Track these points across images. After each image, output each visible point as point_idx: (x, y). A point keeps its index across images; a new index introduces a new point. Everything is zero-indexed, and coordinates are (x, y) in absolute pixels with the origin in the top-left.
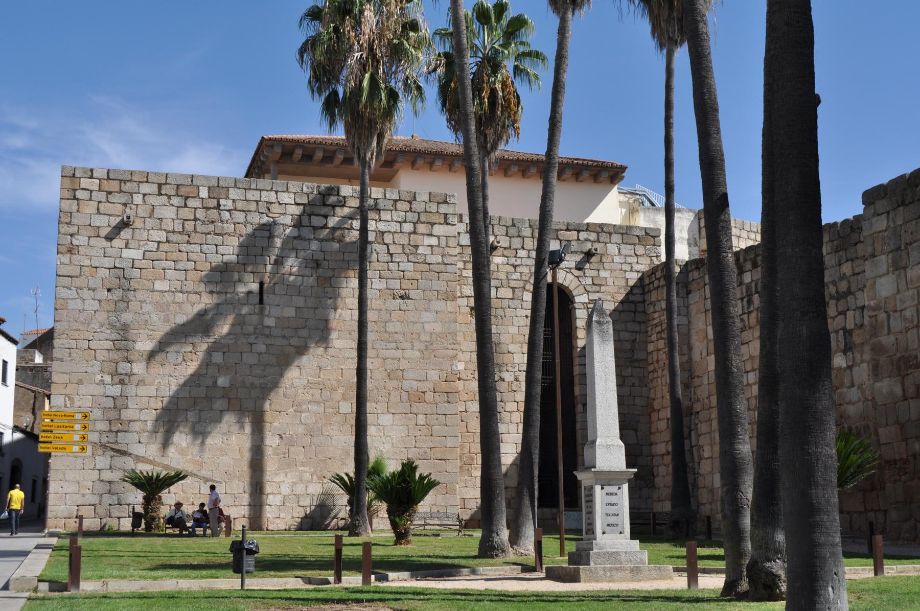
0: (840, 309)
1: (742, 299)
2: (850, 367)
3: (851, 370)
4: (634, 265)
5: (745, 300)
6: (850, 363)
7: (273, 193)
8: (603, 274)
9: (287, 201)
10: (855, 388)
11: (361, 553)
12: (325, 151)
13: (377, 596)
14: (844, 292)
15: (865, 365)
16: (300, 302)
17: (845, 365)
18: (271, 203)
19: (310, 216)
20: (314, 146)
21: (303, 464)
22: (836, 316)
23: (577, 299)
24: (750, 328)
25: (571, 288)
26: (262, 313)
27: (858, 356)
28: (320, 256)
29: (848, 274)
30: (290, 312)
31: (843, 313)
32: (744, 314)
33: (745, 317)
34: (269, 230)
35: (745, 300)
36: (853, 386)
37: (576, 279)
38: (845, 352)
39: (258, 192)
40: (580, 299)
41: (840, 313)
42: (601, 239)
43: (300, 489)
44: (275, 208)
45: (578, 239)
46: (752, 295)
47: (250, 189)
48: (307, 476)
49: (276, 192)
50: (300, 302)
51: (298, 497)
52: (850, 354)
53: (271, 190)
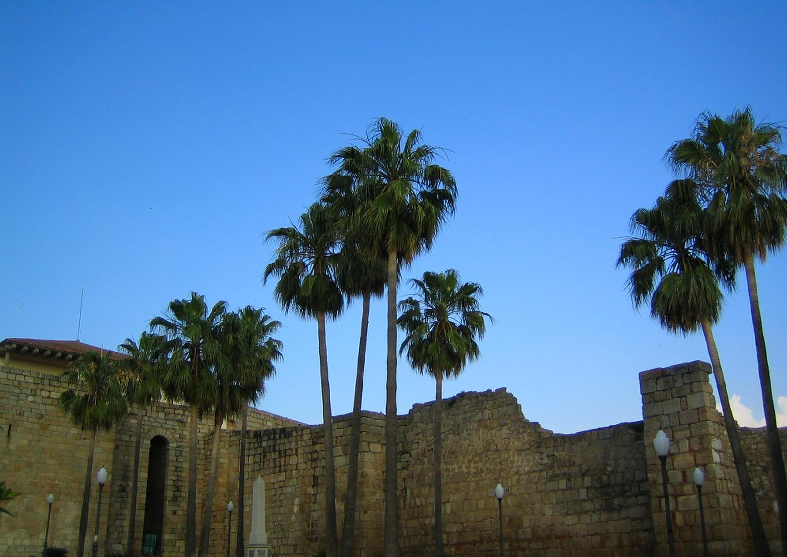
0: (313, 466)
1: (260, 454)
2: (315, 494)
3: (316, 496)
4: (201, 429)
5: (262, 455)
6: (316, 492)
7: (23, 377)
8: (185, 433)
9: (152, 421)
10: (317, 504)
11: (766, 425)
12: (29, 347)
13: (254, 546)
14: (316, 459)
15: (323, 494)
16: (31, 437)
17: (313, 493)
18: (21, 381)
19: (41, 390)
20: (23, 344)
21: (22, 528)
22: (310, 469)
23: (171, 445)
24: (264, 469)
25: (168, 439)
26: (9, 442)
27: (319, 489)
28: (44, 413)
29: (318, 450)
30: (24, 442)
31: (315, 468)
32: (260, 461)
33: (262, 463)
34: (18, 396)
35: (262, 455)
36: (316, 503)
37: (171, 434)
38: (313, 486)
39: (15, 375)
40: (173, 445)
41: (312, 468)
42: (186, 414)
43: (18, 542)
44: (23, 385)
45: (174, 413)
46: (266, 453)
47: (10, 373)
48: (23, 535)
49: (25, 376)
50: (31, 437)
51: (16, 547)
52: (316, 488)
53: (22, 374)
